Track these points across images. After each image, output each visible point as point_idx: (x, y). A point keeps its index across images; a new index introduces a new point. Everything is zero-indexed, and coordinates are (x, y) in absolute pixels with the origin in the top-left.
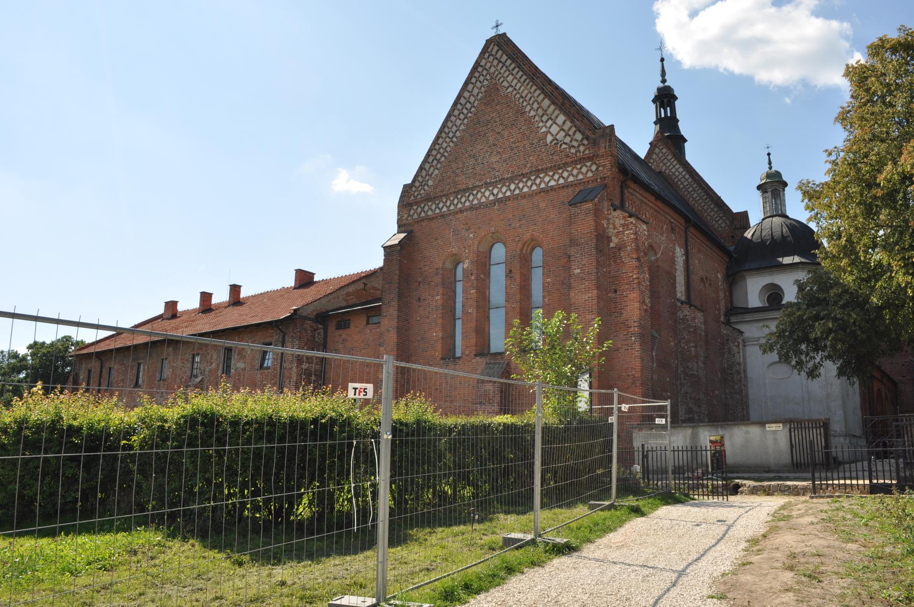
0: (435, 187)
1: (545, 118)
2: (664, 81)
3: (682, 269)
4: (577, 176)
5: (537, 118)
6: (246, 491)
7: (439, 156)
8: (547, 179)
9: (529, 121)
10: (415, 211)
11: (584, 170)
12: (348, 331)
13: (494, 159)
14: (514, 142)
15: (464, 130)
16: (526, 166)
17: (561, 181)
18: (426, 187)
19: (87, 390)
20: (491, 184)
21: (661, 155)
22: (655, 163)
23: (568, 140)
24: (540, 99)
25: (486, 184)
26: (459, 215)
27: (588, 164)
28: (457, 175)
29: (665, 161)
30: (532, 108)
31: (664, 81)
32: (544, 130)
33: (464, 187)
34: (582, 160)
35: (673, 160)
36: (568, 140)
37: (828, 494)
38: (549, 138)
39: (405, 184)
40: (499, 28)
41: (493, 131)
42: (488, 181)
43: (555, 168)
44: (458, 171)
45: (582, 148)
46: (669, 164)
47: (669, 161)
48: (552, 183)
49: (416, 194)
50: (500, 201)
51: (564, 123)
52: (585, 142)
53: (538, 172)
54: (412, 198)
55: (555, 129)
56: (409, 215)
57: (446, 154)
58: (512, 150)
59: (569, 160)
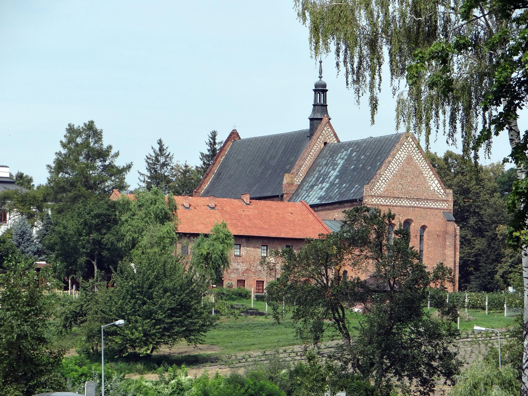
0: (384, 192)
1: (431, 179)
2: (320, 77)
5: (427, 178)
6: (121, 322)
9: (425, 178)
14: (418, 184)
15: (397, 171)
18: (379, 191)
19: (32, 237)
21: (327, 132)
24: (425, 163)
26: (395, 208)
27: (445, 203)
28: (394, 190)
29: (329, 137)
33: (397, 196)
34: (443, 201)
35: (334, 137)
37: (47, 390)
38: (432, 188)
42: (408, 197)
45: (443, 196)
46: (331, 139)
47: (332, 137)
49: (375, 192)
52: (445, 194)
53: (427, 200)
54: (373, 193)
55: (434, 185)
57: (386, 183)
58: (418, 187)
59: (439, 199)
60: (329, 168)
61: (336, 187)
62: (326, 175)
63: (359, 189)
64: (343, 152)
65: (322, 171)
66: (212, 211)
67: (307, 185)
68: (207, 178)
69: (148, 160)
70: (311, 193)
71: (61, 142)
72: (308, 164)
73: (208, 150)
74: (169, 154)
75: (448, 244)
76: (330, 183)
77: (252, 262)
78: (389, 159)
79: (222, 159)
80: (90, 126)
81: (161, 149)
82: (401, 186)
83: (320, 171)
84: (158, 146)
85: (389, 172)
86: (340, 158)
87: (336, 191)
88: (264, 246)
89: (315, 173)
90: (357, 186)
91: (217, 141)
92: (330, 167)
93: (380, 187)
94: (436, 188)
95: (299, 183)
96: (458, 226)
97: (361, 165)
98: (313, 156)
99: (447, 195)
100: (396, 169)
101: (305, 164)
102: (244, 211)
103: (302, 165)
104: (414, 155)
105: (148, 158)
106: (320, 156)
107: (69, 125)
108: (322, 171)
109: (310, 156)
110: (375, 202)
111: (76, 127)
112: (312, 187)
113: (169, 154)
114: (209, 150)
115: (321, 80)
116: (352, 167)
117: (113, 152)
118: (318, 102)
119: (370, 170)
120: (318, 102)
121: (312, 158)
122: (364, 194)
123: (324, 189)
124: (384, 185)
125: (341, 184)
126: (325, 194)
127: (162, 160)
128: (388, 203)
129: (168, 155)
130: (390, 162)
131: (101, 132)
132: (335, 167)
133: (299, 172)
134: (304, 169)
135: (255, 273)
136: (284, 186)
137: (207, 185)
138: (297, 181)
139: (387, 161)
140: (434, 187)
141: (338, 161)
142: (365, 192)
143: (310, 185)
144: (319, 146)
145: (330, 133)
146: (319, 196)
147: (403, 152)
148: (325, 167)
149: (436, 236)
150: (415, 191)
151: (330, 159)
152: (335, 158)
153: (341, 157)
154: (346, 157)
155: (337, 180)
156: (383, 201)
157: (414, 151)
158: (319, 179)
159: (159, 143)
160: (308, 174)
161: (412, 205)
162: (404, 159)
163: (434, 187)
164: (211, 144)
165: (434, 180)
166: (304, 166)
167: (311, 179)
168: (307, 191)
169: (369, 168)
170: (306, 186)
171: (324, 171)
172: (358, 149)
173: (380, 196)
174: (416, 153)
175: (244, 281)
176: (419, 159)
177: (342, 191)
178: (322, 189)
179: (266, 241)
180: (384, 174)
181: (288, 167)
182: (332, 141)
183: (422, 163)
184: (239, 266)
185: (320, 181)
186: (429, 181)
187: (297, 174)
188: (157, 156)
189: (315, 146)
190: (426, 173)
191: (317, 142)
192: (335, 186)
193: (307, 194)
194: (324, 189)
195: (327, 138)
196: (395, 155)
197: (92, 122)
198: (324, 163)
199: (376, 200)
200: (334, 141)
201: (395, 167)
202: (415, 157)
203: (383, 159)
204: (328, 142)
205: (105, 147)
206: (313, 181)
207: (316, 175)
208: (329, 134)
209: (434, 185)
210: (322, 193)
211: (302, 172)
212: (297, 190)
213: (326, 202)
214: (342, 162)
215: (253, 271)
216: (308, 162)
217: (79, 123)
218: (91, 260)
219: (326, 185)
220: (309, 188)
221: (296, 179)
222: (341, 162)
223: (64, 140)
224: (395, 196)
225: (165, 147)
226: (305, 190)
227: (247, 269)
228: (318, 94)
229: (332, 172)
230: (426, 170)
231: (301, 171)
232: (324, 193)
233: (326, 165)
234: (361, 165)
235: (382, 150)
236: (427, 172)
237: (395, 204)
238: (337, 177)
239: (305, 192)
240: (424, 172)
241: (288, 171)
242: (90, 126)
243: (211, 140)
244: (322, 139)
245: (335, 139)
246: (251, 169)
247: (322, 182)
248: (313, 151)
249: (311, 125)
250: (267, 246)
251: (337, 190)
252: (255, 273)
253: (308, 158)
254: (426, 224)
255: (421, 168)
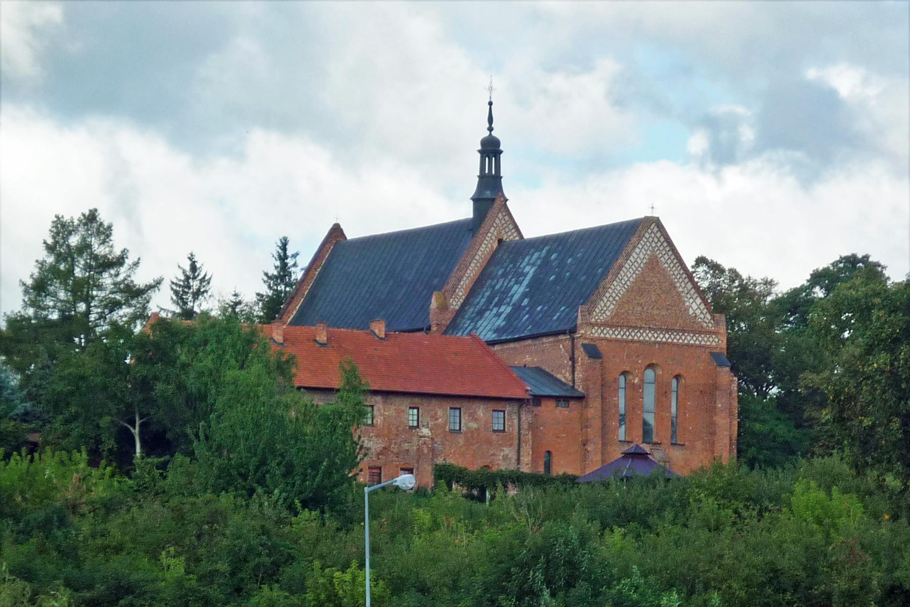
1: (689, 296)
2: (490, 129)
3: (544, 368)
4: (707, 342)
5: (683, 294)
7: (614, 295)
8: (689, 338)
9: (679, 294)
10: (596, 331)
11: (711, 339)
12: (539, 408)
13: (655, 312)
14: (669, 305)
16: (676, 325)
17: (697, 342)
20: (653, 329)
22: (498, 228)
23: (702, 316)
24: (679, 269)
25: (649, 328)
26: (631, 345)
27: (714, 336)
29: (507, 230)
30: (681, 286)
31: (490, 129)
32: (687, 304)
33: (634, 325)
34: (711, 333)
35: (513, 231)
36: (702, 316)
39: (340, 224)
40: (654, 210)
41: (654, 291)
43: (694, 332)
44: (630, 312)
45: (710, 325)
46: (510, 234)
47: (510, 230)
48: (692, 342)
49: (597, 318)
50: (659, 343)
51: (700, 304)
52: (712, 321)
53: (683, 331)
54: (593, 320)
55: (694, 306)
56: (592, 333)
57: (614, 302)
58: (667, 310)
59: (703, 330)
60: (510, 281)
61: (525, 312)
62: (506, 292)
63: (568, 314)
64: (532, 255)
65: (497, 287)
66: (322, 349)
67: (471, 310)
68: (293, 305)
69: (175, 287)
70: (480, 323)
71: (45, 242)
72: (471, 275)
73: (275, 266)
74: (206, 275)
75: (720, 405)
76: (513, 305)
77: (393, 437)
78: (619, 261)
79: (317, 273)
80: (91, 217)
81: (194, 268)
82: (640, 308)
83: (494, 287)
84: (189, 262)
85: (620, 284)
86: (528, 264)
87: (525, 318)
88: (413, 408)
89: (484, 289)
90: (562, 308)
91: (289, 253)
92: (512, 278)
93: (605, 308)
94: (698, 312)
95: (457, 308)
96: (735, 376)
97: (568, 274)
98: (480, 261)
99: (717, 323)
100: (631, 279)
101: (467, 275)
102: (375, 349)
103: (463, 277)
104: (660, 255)
105: (173, 283)
106: (493, 259)
107: (57, 217)
108: (497, 287)
109: (474, 261)
110: (596, 335)
111: (67, 218)
112: (480, 313)
113: (206, 275)
114: (276, 267)
115: (490, 134)
116: (551, 278)
117: (129, 262)
118: (487, 172)
119: (585, 282)
120: (487, 172)
121: (478, 265)
122: (579, 321)
123: (503, 316)
124: (612, 307)
125: (533, 306)
126: (506, 324)
127: (195, 284)
128: (619, 337)
129: (204, 277)
130: (621, 267)
131: (110, 228)
132: (521, 278)
133: (456, 288)
134: (465, 283)
135: (397, 455)
136: (432, 312)
137: (292, 317)
138: (454, 303)
139: (616, 266)
140: (695, 308)
141: (524, 267)
142: (580, 317)
143: (476, 310)
144: (489, 245)
145: (509, 223)
146: (495, 327)
147: (643, 250)
148: (501, 281)
149: (698, 393)
150: (663, 316)
151: (511, 266)
152: (518, 264)
153: (531, 262)
154: (539, 262)
155: (526, 301)
156: (611, 332)
157: (661, 248)
158: (494, 299)
159: (189, 258)
160: (473, 292)
161: (659, 339)
162: (645, 261)
163: (695, 308)
164: (280, 256)
165: (694, 297)
166: (465, 278)
167: (478, 300)
168: (472, 320)
169: (583, 278)
170: (471, 311)
171: (501, 287)
172: (560, 248)
173: (605, 325)
174: (664, 252)
175: (380, 468)
176: (669, 262)
177: (538, 318)
178: (498, 315)
179: (417, 400)
180: (612, 286)
181: (436, 281)
182: (512, 237)
183: (674, 269)
184: (372, 443)
185: (494, 302)
186: (686, 299)
187: (454, 291)
188: (187, 278)
189: (483, 245)
190: (681, 286)
191: (487, 238)
192: (523, 310)
193: (472, 324)
194: (503, 316)
195: (503, 232)
196: (629, 255)
197: (96, 210)
198: (500, 272)
199: (599, 331)
200: (514, 237)
201: (629, 275)
202: (662, 259)
203: (607, 262)
204: (504, 239)
205: (117, 252)
206: (481, 304)
207: (487, 294)
208: (505, 225)
209: (694, 306)
210: (500, 322)
211: (462, 289)
212: (454, 320)
213: (509, 337)
214: (534, 269)
215: (395, 451)
216: (472, 271)
217: (74, 213)
218: (129, 427)
219: (506, 310)
220: (474, 315)
221: (452, 300)
222: (530, 271)
223: (50, 241)
224: (630, 324)
225: (198, 265)
226: (468, 319)
227: (384, 448)
228: (487, 159)
229: (516, 287)
230: (681, 280)
231: (460, 287)
232: (504, 323)
233: (504, 275)
234: (568, 274)
235: (605, 246)
236: (683, 285)
237: (630, 338)
238: (524, 295)
239: (469, 321)
240: (678, 285)
241: (438, 288)
242: (91, 217)
243: (280, 251)
244: (495, 233)
245: (515, 234)
246: (369, 288)
247: (499, 305)
248: (480, 253)
249: (476, 210)
250: (418, 409)
251: (527, 316)
252: (397, 455)
253: (472, 265)
254: (682, 373)
255: (674, 277)
